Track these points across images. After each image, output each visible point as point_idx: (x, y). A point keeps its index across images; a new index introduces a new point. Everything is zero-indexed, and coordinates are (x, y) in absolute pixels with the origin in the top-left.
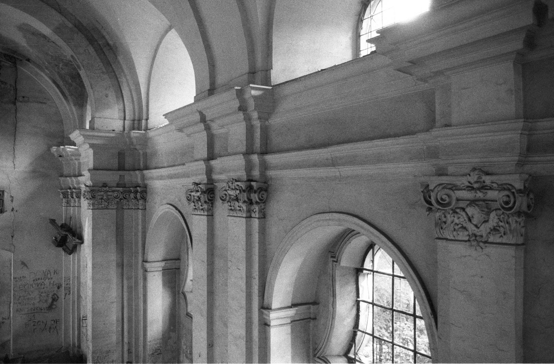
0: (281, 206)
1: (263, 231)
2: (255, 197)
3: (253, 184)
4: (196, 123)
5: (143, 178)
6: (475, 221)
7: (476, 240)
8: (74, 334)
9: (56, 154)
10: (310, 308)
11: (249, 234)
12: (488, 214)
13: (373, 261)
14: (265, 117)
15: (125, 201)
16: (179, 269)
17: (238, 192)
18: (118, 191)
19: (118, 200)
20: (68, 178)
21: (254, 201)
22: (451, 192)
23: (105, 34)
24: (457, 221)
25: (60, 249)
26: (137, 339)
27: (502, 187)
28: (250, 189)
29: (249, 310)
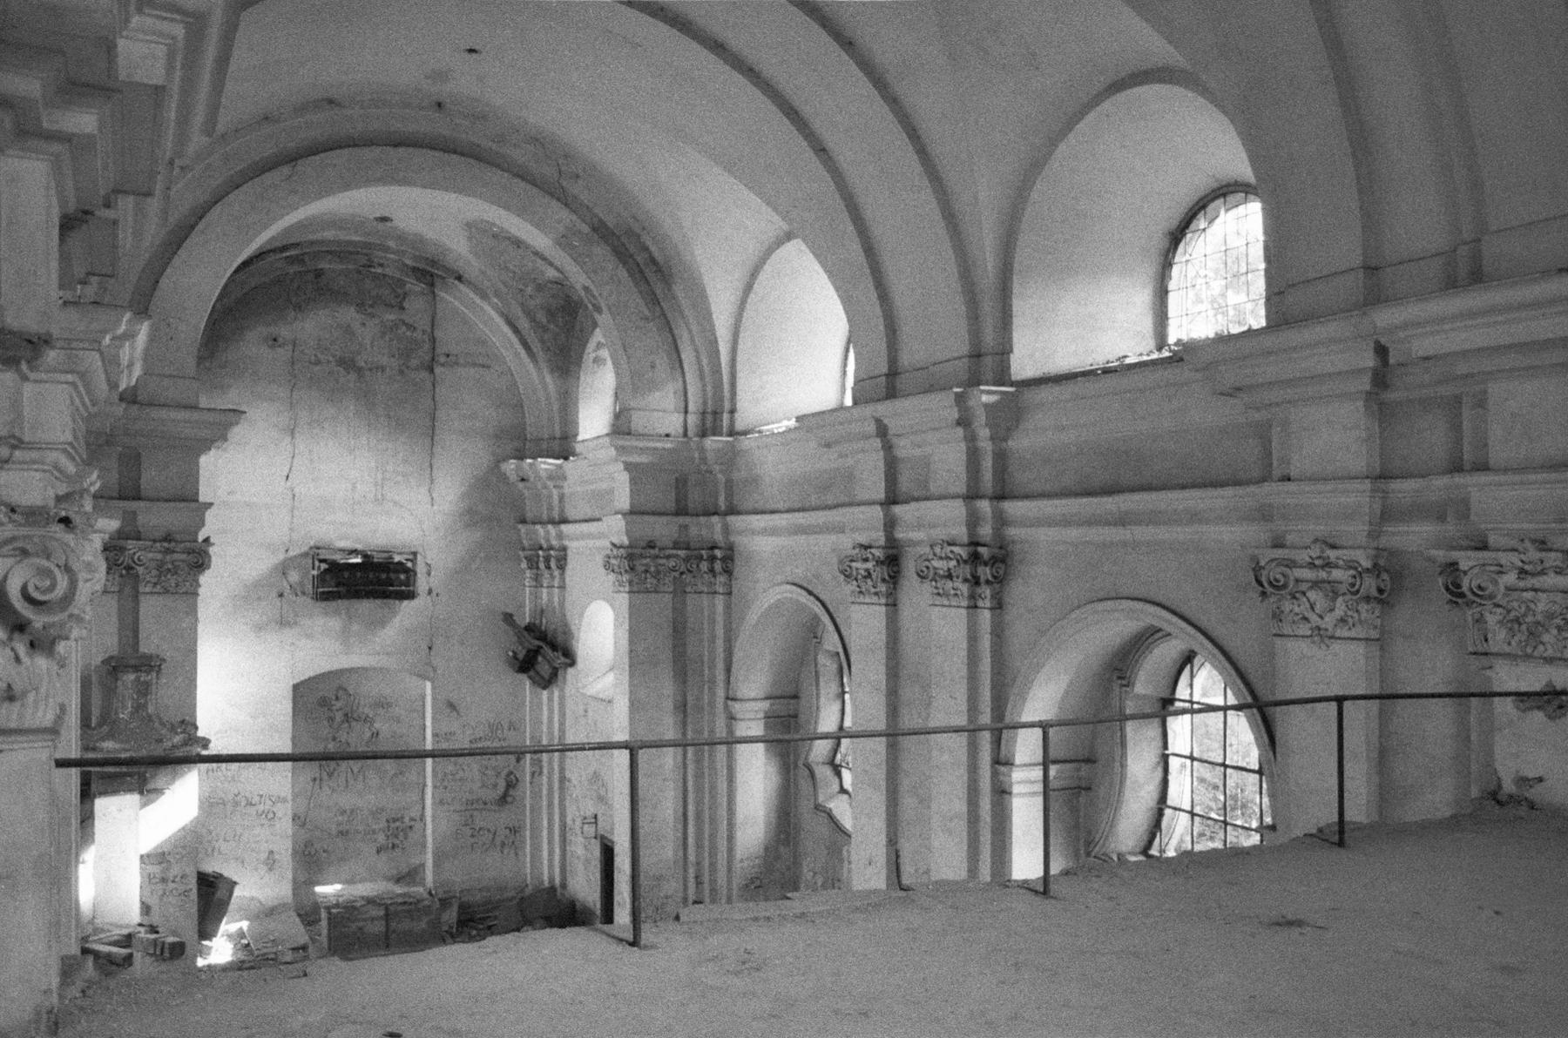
0: (1031, 590)
1: (998, 633)
2: (985, 572)
3: (981, 549)
4: (867, 438)
5: (726, 530)
6: (1318, 608)
7: (1321, 635)
8: (551, 861)
9: (513, 477)
10: (1079, 770)
11: (973, 638)
12: (1334, 600)
13: (1191, 686)
14: (1000, 436)
15: (687, 578)
16: (796, 716)
17: (953, 563)
18: (676, 556)
19: (677, 574)
20: (538, 527)
21: (982, 579)
22: (1288, 571)
23: (649, 243)
24: (1297, 610)
25: (523, 677)
26: (713, 853)
27: (1351, 565)
28: (975, 558)
29: (973, 768)
